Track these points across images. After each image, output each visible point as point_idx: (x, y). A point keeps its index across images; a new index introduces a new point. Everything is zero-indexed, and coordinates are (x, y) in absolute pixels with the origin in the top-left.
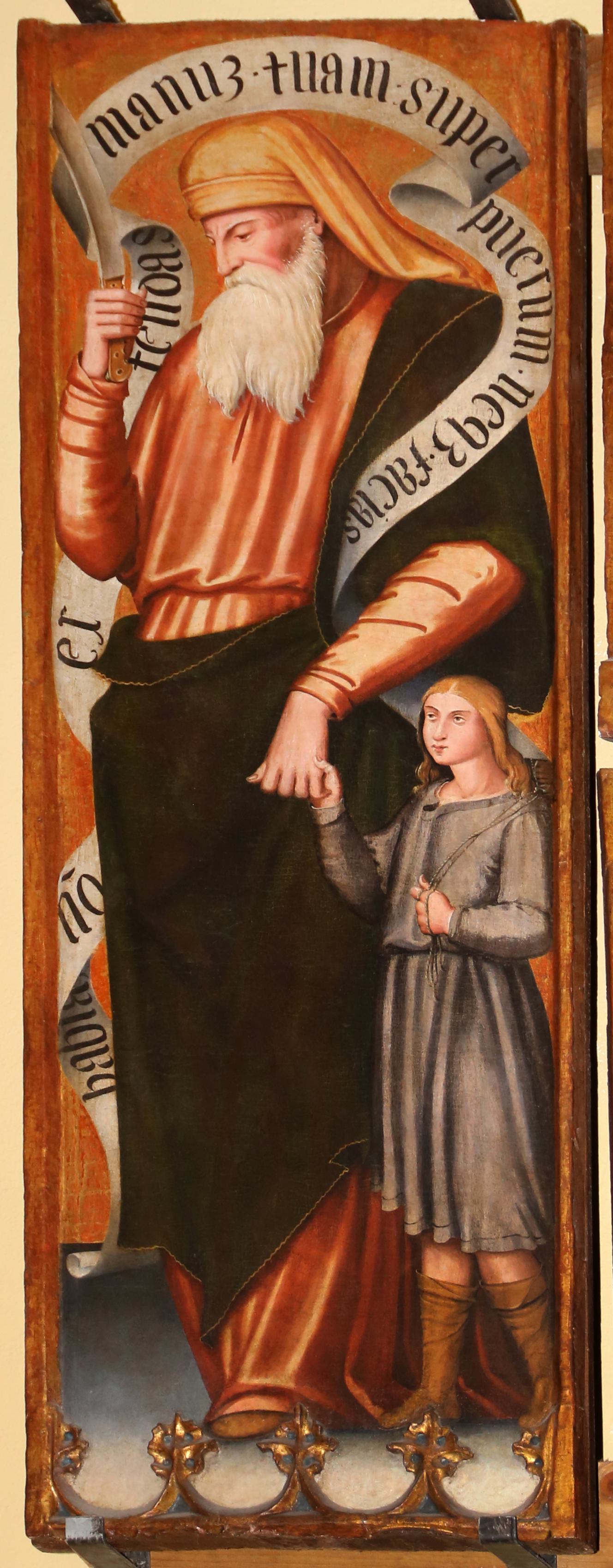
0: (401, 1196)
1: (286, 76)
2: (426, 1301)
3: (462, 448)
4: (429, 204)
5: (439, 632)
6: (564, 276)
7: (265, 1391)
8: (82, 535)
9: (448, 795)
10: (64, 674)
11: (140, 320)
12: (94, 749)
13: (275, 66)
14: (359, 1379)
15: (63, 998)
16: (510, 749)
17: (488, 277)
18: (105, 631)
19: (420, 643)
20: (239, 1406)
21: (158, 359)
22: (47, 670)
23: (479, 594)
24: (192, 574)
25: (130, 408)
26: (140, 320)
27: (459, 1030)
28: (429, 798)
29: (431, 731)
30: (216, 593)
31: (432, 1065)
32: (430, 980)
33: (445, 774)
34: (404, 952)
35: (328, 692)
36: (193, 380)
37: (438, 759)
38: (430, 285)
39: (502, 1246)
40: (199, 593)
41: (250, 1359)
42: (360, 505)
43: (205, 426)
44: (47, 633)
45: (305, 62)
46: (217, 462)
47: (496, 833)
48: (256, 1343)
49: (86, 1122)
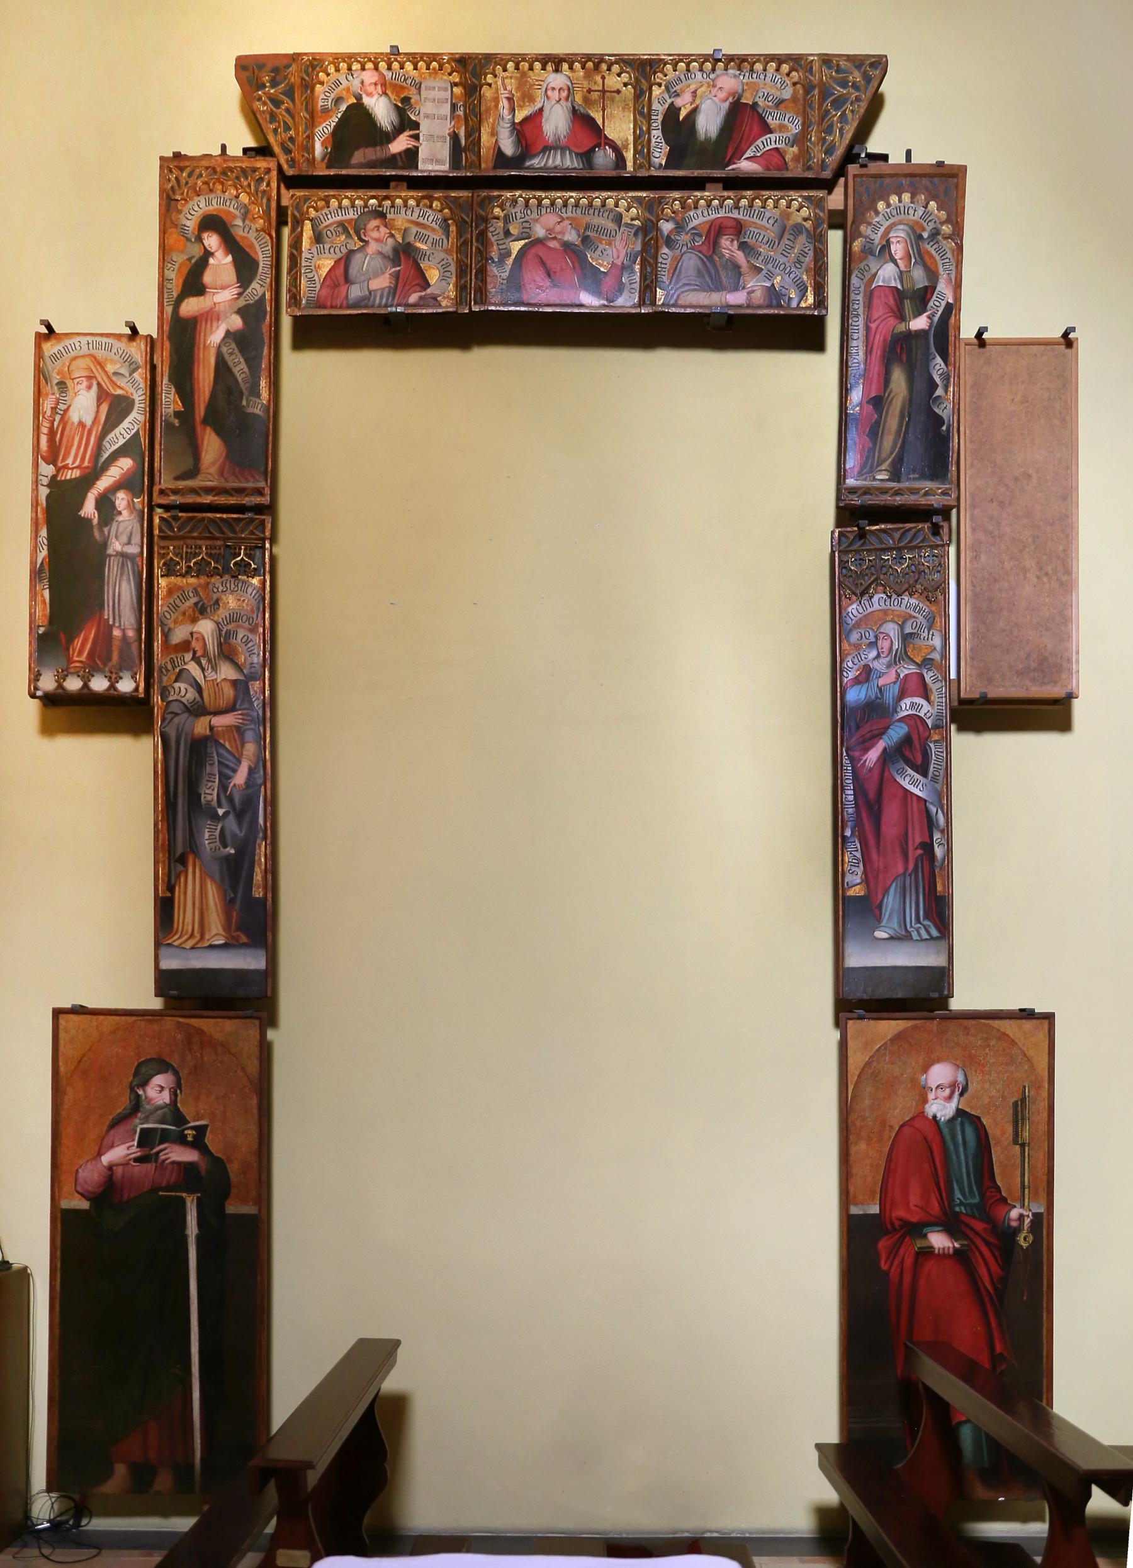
0: (108, 615)
1: (91, 346)
2: (113, 640)
3: (126, 435)
4: (120, 376)
5: (120, 479)
6: (148, 394)
7: (79, 661)
8: (44, 454)
9: (120, 518)
10: (40, 487)
11: (58, 403)
12: (47, 505)
13: (88, 344)
14: (99, 659)
15: (38, 566)
16: (134, 507)
17: (132, 394)
18: (49, 477)
19: (115, 481)
20: (72, 665)
21: (62, 412)
22: (37, 486)
23: (128, 470)
24: (68, 464)
25: (56, 424)
26: (58, 403)
27: (122, 575)
28: (117, 519)
29: (117, 503)
30: (73, 469)
31: (116, 583)
32: (116, 563)
33: (120, 513)
34: (110, 556)
35: (96, 493)
36: (69, 418)
37: (119, 509)
38: (119, 396)
39: (129, 627)
40: (69, 469)
41: (75, 654)
42: (104, 448)
43: (71, 429)
44: (37, 478)
45: (95, 342)
46: (73, 438)
47: (130, 527)
48: (77, 650)
49: (42, 596)
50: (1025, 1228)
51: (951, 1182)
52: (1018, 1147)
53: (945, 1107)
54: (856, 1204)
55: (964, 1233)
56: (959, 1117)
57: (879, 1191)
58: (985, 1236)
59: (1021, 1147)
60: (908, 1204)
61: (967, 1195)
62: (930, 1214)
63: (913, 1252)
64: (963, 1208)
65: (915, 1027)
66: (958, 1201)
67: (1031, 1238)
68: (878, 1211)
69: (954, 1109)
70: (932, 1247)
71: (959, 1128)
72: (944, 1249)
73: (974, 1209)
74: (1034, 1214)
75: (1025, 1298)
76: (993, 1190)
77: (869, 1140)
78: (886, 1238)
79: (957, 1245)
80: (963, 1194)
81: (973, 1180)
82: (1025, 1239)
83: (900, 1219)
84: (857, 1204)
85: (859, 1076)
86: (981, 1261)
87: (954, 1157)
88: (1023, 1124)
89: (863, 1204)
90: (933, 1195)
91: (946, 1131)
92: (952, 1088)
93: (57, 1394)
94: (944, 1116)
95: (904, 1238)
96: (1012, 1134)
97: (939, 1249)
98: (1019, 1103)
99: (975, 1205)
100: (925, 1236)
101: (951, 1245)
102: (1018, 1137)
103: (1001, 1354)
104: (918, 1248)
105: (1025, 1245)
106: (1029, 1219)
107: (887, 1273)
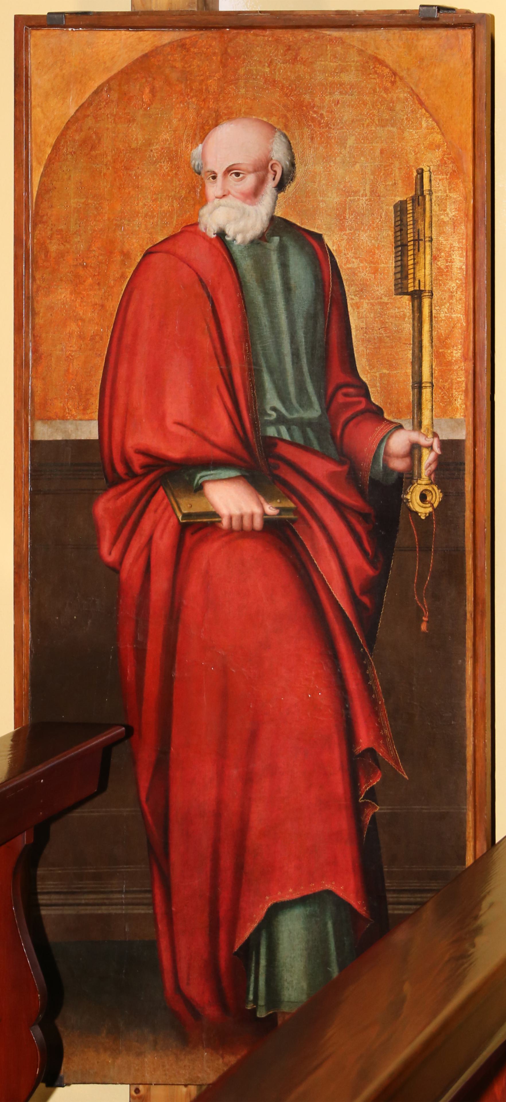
50: (425, 473)
51: (259, 372)
52: (406, 299)
53: (244, 214)
54: (47, 419)
55: (285, 484)
56: (273, 235)
57: (97, 390)
58: (333, 490)
59: (413, 301)
60: (162, 419)
61: (294, 401)
63: (173, 521)
64: (283, 429)
65: (182, 45)
66: (274, 415)
67: (436, 497)
68: (95, 435)
70: (215, 514)
71: (274, 257)
72: (242, 517)
73: (311, 434)
74: (444, 444)
75: (424, 627)
76: (351, 390)
77: (77, 281)
78: (112, 493)
79: (271, 510)
80: (283, 396)
81: (305, 369)
82: (423, 497)
83: (145, 453)
84: (50, 419)
85: (56, 147)
86: (323, 543)
87: (264, 320)
88: (417, 249)
89: (64, 418)
90: (217, 400)
91: (246, 264)
92: (261, 173)
94: (242, 232)
97: (231, 518)
98: (410, 207)
99: (310, 423)
100: (200, 489)
101: (257, 510)
102: (406, 277)
103: (371, 751)
104: (185, 516)
105: (423, 510)
106: (432, 456)
107: (115, 569)
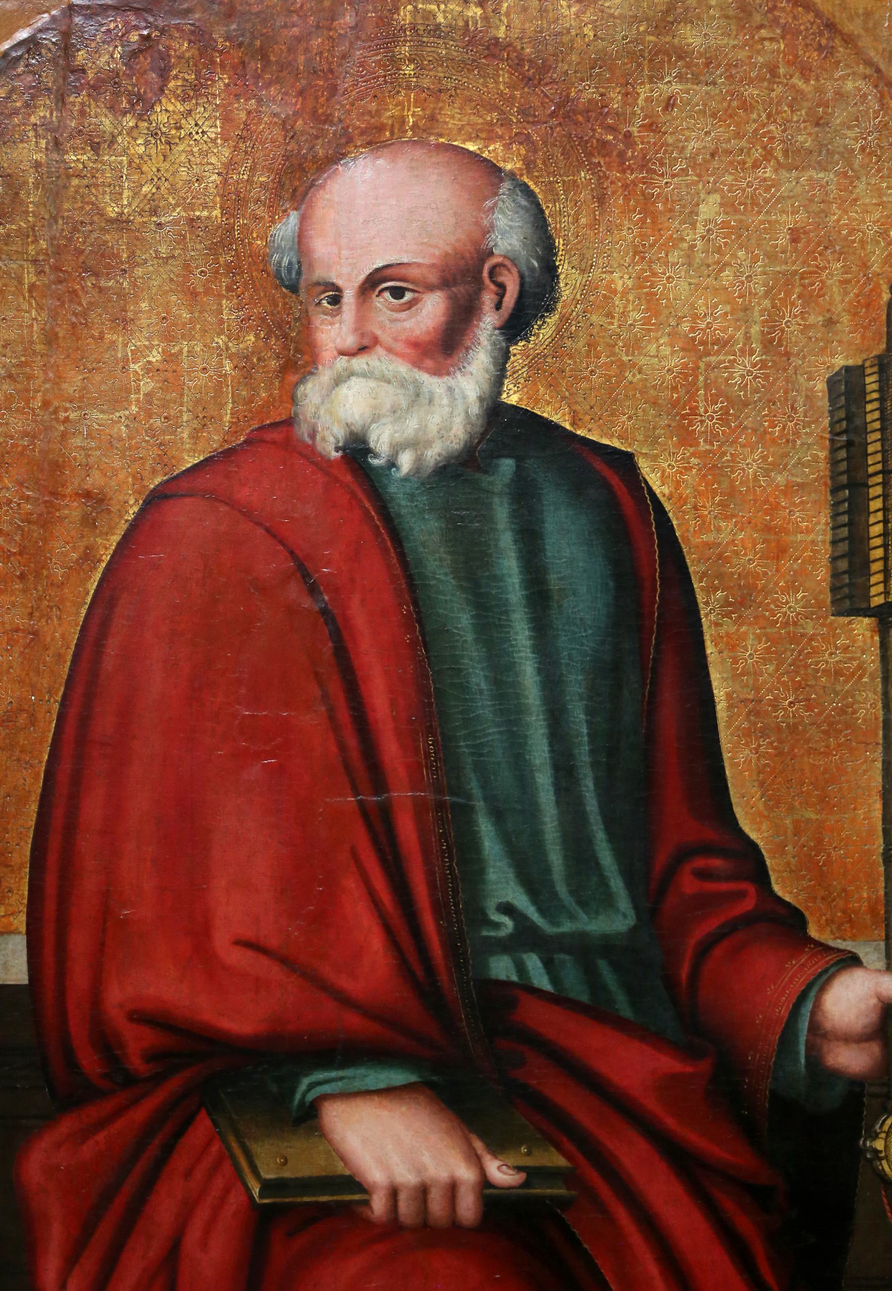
51: (465, 812)
52: (863, 626)
58: (670, 1122)
61: (562, 889)
62: (324, 986)
63: (235, 1200)
64: (533, 962)
66: (508, 923)
69: (475, 409)
71: (502, 512)
72: (423, 1191)
76: (717, 863)
78: (66, 1126)
81: (592, 805)
90: (351, 884)
93: (43, 1145)
94: (413, 444)
95: (180, 1133)
96: (825, 552)
97: (394, 1193)
98: (871, 382)
101: (466, 1174)
104: (268, 1187)
